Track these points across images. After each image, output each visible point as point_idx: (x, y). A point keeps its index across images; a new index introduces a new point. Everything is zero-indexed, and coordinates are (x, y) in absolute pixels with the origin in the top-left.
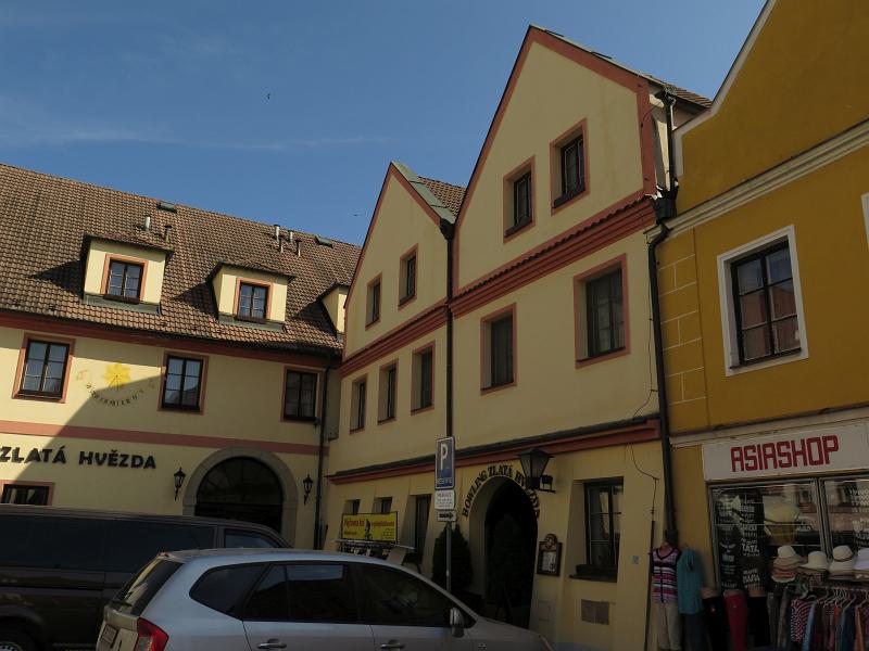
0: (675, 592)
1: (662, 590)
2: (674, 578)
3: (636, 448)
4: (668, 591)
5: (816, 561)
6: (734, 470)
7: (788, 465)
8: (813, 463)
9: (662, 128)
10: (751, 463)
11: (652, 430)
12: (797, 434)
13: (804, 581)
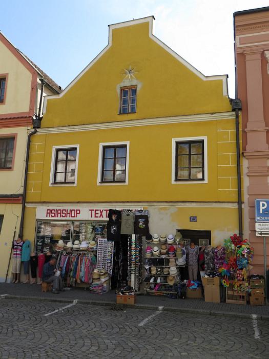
0: (21, 255)
1: (16, 254)
2: (21, 250)
3: (7, 205)
4: (19, 254)
5: (69, 245)
6: (47, 216)
7: (65, 216)
8: (72, 217)
9: (39, 91)
10: (53, 215)
11: (20, 200)
12: (69, 208)
13: (65, 250)
